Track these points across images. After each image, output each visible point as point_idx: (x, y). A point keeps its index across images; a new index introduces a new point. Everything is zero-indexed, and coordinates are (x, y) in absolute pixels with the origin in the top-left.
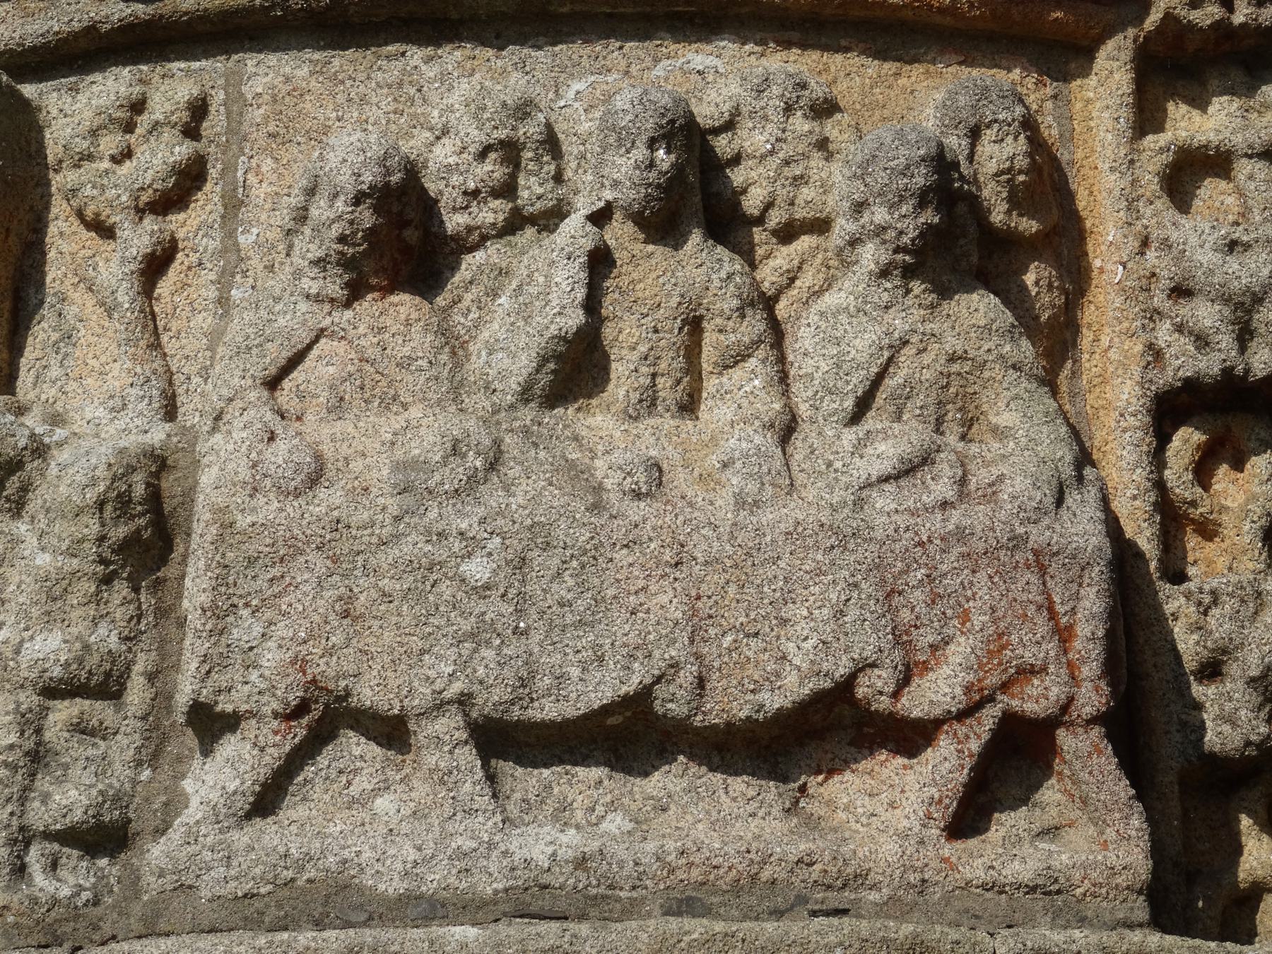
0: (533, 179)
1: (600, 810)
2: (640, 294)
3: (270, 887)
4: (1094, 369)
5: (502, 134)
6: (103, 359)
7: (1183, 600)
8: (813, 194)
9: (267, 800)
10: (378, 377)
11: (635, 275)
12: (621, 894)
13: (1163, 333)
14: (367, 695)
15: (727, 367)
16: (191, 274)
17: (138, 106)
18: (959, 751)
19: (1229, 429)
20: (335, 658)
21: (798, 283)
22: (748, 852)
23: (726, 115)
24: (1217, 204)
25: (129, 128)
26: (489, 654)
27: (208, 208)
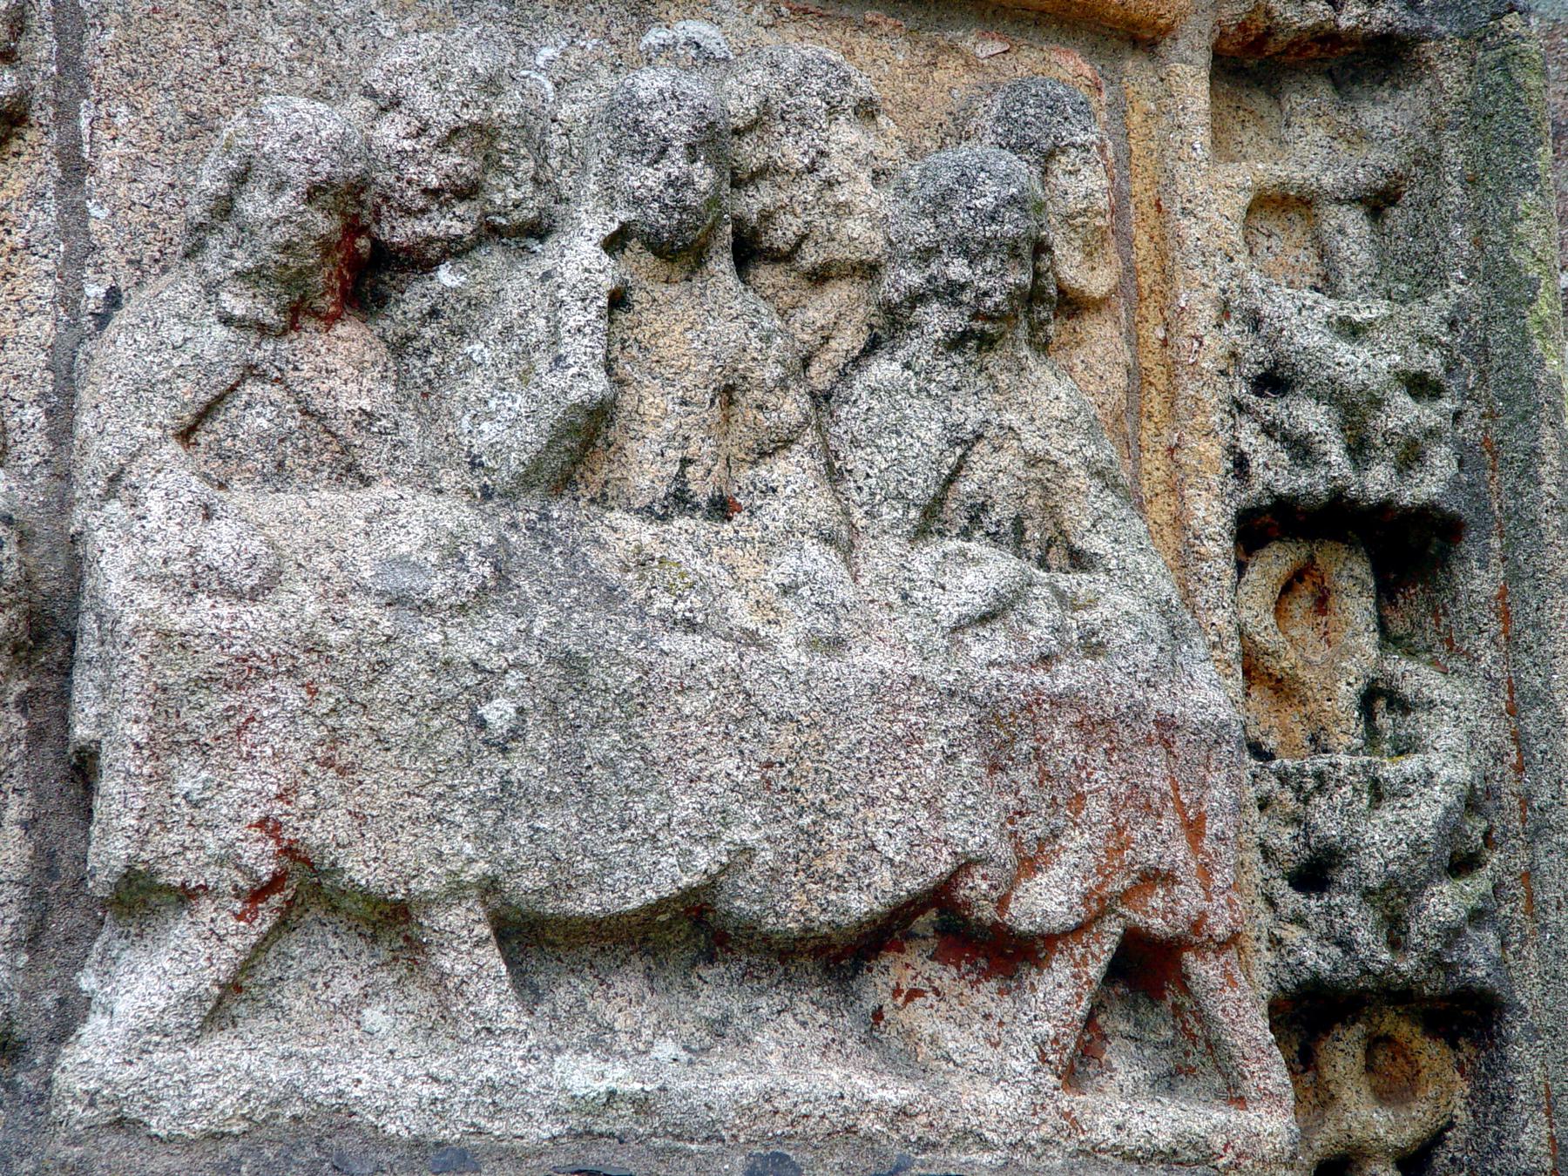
0: (507, 179)
1: (647, 1033)
2: (664, 353)
3: (244, 1125)
4: (1156, 473)
5: (472, 115)
7: (1275, 782)
8: (859, 229)
9: (225, 1004)
10: (326, 438)
11: (657, 326)
12: (694, 1147)
13: (1248, 437)
14: (362, 869)
15: (763, 454)
16: (16, 259)
18: (1075, 976)
19: (1311, 557)
20: (318, 821)
21: (833, 343)
22: (842, 1097)
23: (753, 111)
24: (1291, 260)
26: (520, 826)
27: (37, 167)
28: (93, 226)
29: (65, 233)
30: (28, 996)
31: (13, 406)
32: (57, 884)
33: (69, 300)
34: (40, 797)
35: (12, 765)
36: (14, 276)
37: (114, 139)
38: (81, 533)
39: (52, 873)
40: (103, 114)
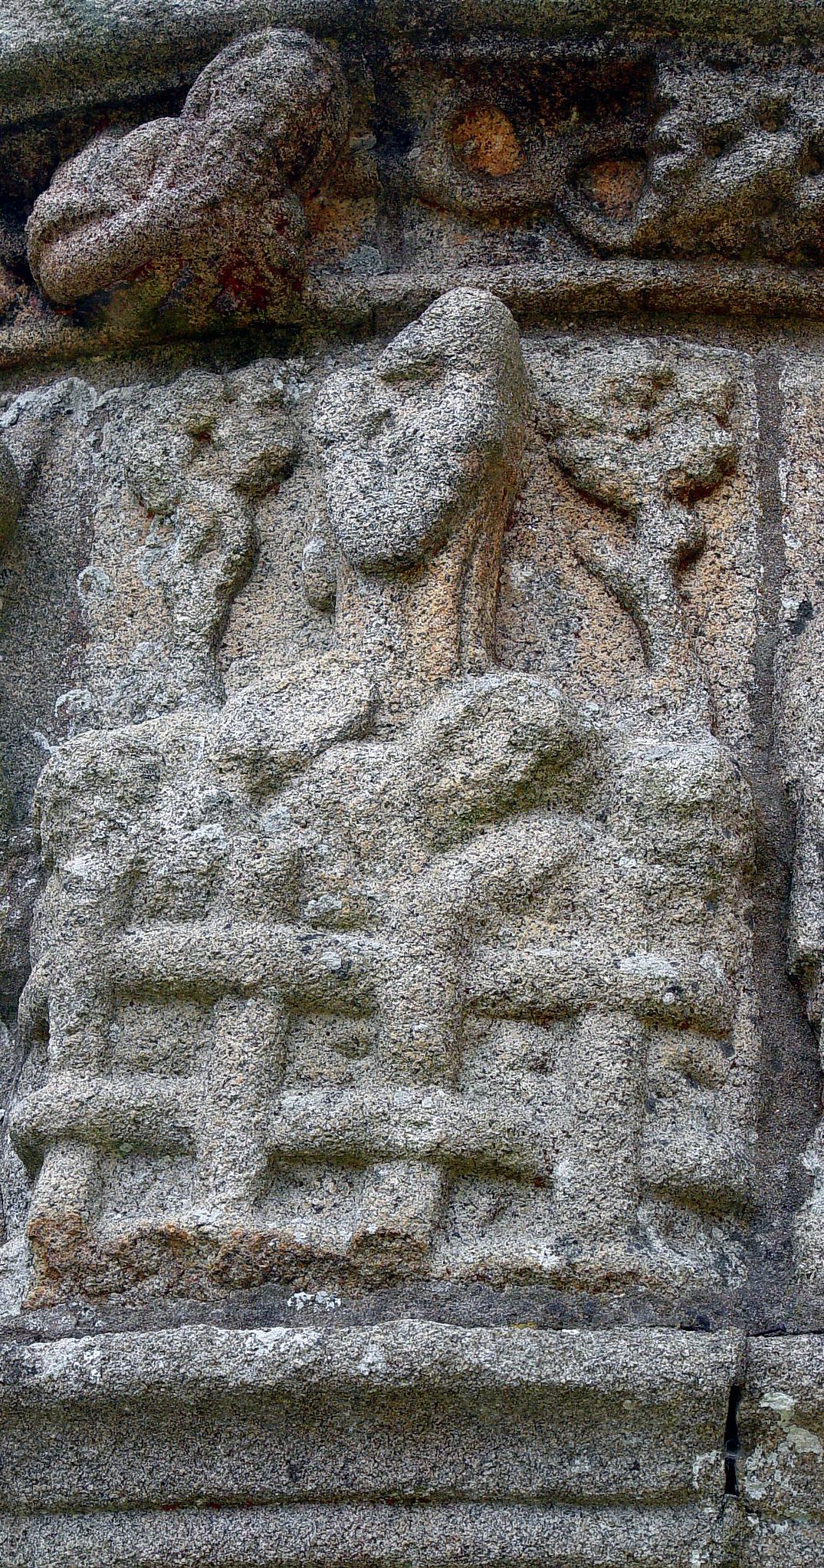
6: (616, 655)
17: (661, 381)
25: (648, 404)
28: (788, 554)
29: (764, 558)
30: (762, 1167)
31: (722, 690)
32: (781, 1075)
33: (768, 610)
34: (763, 998)
35: (742, 968)
36: (722, 589)
37: (805, 490)
38: (798, 781)
39: (776, 1065)
40: (797, 470)
